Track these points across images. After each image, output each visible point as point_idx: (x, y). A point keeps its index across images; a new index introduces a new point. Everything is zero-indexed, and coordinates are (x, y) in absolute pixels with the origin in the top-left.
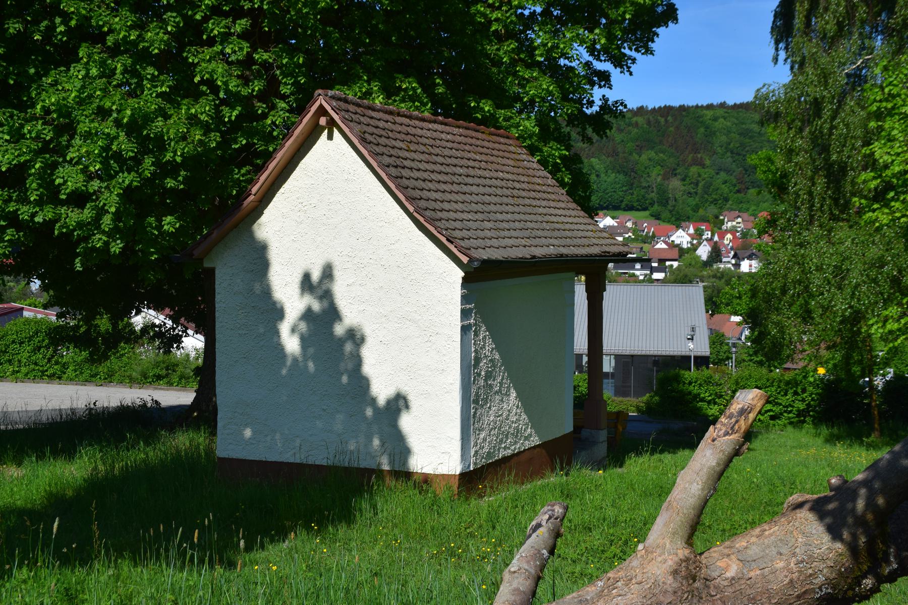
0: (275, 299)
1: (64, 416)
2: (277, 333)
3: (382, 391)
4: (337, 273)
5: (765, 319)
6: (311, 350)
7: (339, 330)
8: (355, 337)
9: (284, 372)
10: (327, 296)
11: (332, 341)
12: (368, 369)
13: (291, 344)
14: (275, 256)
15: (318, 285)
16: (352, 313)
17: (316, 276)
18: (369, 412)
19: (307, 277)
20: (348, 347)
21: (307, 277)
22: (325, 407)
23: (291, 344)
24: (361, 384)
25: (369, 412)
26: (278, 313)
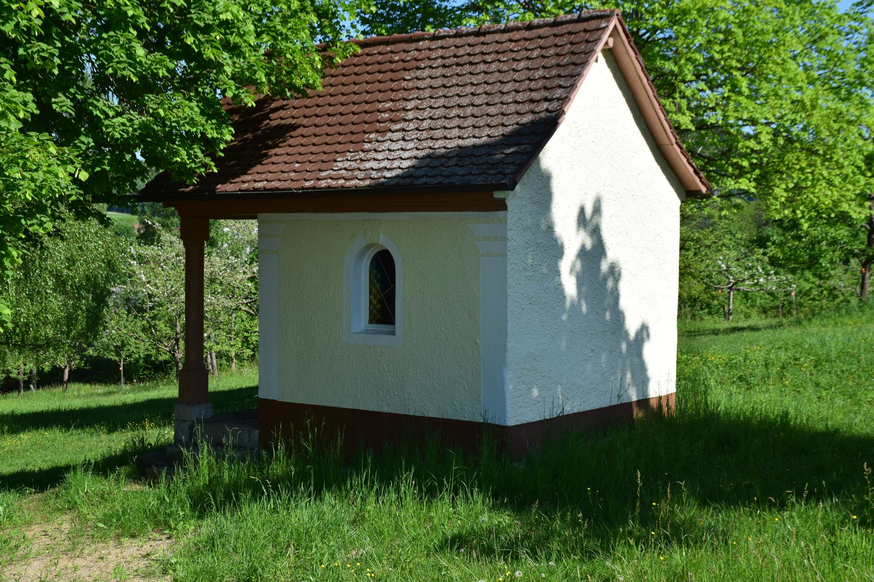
0: (620, 308)
1: (798, 421)
2: (558, 273)
3: (632, 326)
4: (605, 208)
5: (676, 490)
6: (584, 289)
7: (604, 266)
8: (614, 272)
9: (564, 318)
10: (596, 232)
11: (598, 274)
12: (624, 303)
13: (570, 285)
14: (558, 187)
15: (590, 221)
16: (614, 252)
17: (589, 211)
18: (624, 346)
19: (582, 211)
20: (610, 283)
21: (582, 211)
22: (593, 347)
23: (570, 285)
24: (619, 317)
25: (624, 346)
26: (557, 250)
